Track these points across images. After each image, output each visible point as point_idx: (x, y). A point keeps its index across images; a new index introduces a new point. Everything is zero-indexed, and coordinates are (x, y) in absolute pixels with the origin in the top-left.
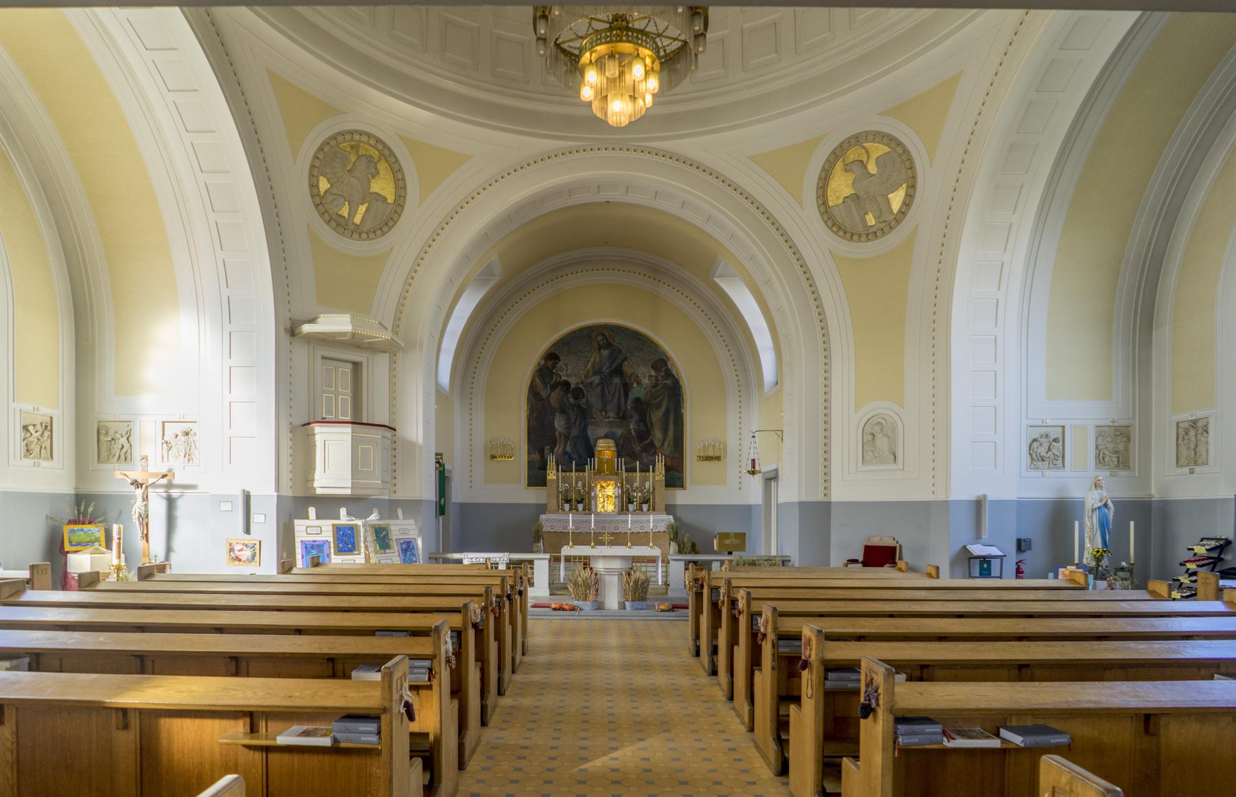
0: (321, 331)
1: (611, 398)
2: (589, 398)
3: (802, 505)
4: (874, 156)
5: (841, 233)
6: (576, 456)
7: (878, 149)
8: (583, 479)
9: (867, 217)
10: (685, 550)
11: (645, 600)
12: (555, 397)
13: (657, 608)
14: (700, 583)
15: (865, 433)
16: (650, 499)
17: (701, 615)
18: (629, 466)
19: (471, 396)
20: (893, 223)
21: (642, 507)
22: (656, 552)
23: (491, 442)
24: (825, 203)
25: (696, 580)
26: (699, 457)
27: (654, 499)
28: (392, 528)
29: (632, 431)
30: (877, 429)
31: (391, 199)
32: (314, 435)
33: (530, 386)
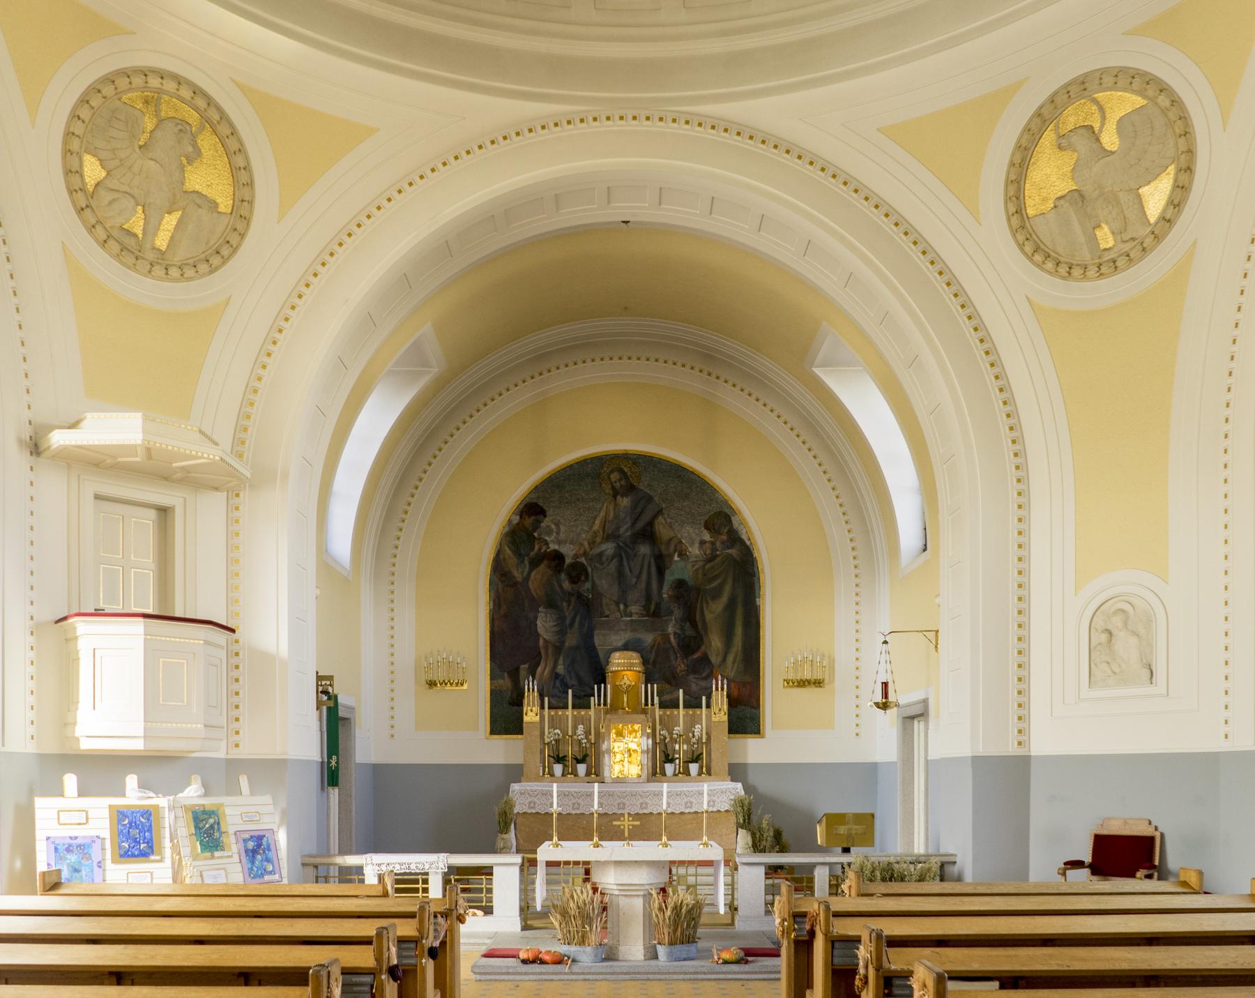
0: (85, 443)
1: (634, 580)
2: (597, 582)
3: (979, 763)
4: (1114, 117)
5: (1050, 265)
6: (574, 682)
7: (1123, 103)
8: (586, 721)
9: (1098, 233)
10: (764, 843)
11: (694, 942)
12: (537, 579)
13: (716, 957)
14: (808, 927)
15: (1092, 630)
16: (702, 753)
17: (808, 992)
18: (667, 697)
19: (392, 578)
20: (1148, 241)
21: (688, 767)
22: (715, 852)
23: (426, 657)
24: (1020, 211)
25: (798, 917)
26: (787, 681)
27: (709, 754)
28: (228, 811)
29: (672, 637)
30: (1117, 621)
31: (225, 204)
32: (76, 638)
33: (493, 561)
